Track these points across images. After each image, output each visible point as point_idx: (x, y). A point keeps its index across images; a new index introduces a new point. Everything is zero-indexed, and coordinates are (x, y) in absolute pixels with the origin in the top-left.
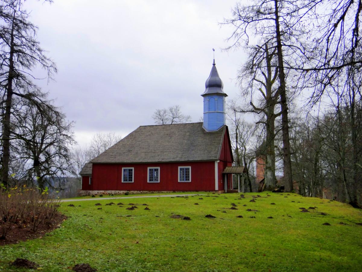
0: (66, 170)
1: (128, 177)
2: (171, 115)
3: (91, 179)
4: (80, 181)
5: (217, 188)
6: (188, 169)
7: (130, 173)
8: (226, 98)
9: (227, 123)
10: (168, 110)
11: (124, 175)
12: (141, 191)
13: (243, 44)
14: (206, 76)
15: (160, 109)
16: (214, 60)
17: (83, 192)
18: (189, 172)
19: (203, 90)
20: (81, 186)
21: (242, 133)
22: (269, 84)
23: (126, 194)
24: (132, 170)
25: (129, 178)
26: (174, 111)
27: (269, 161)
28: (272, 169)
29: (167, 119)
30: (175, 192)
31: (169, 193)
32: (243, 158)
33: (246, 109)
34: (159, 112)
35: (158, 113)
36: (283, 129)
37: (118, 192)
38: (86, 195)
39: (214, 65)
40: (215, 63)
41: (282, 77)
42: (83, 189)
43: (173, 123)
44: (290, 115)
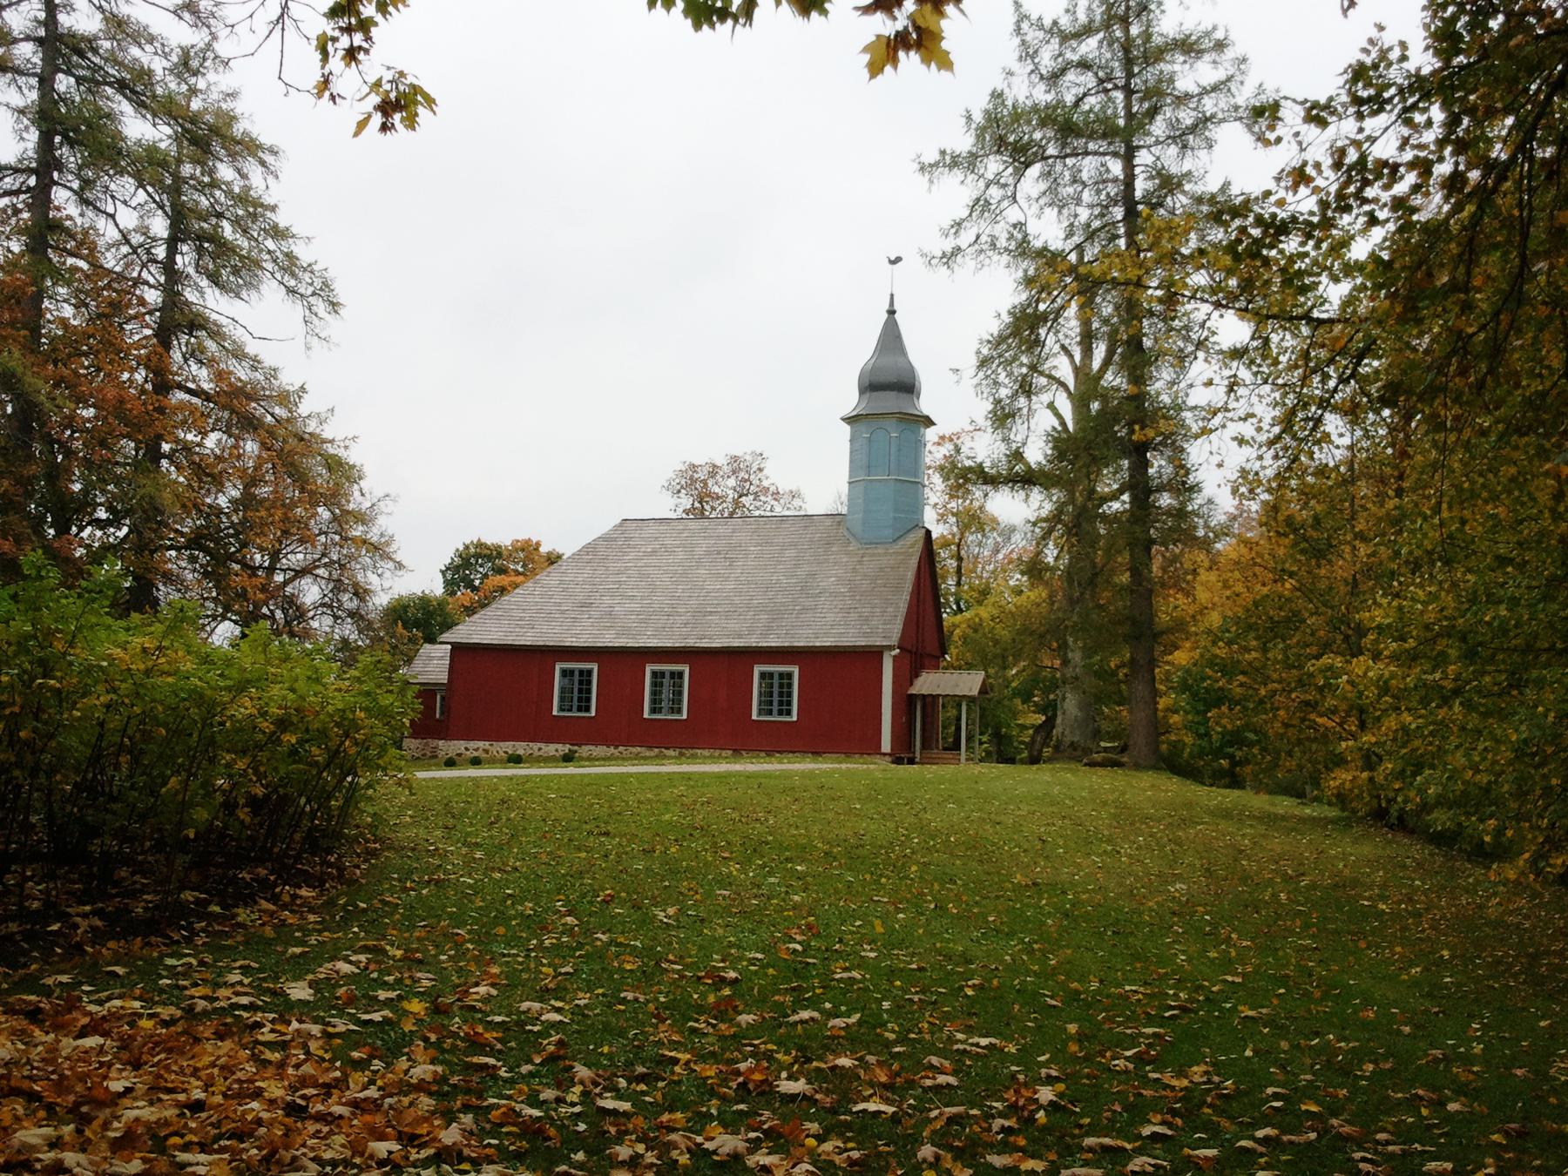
5: (886, 746)
6: (790, 675)
16: (892, 295)
18: (790, 685)
24: (590, 672)
37: (540, 749)
39: (892, 312)
40: (896, 307)
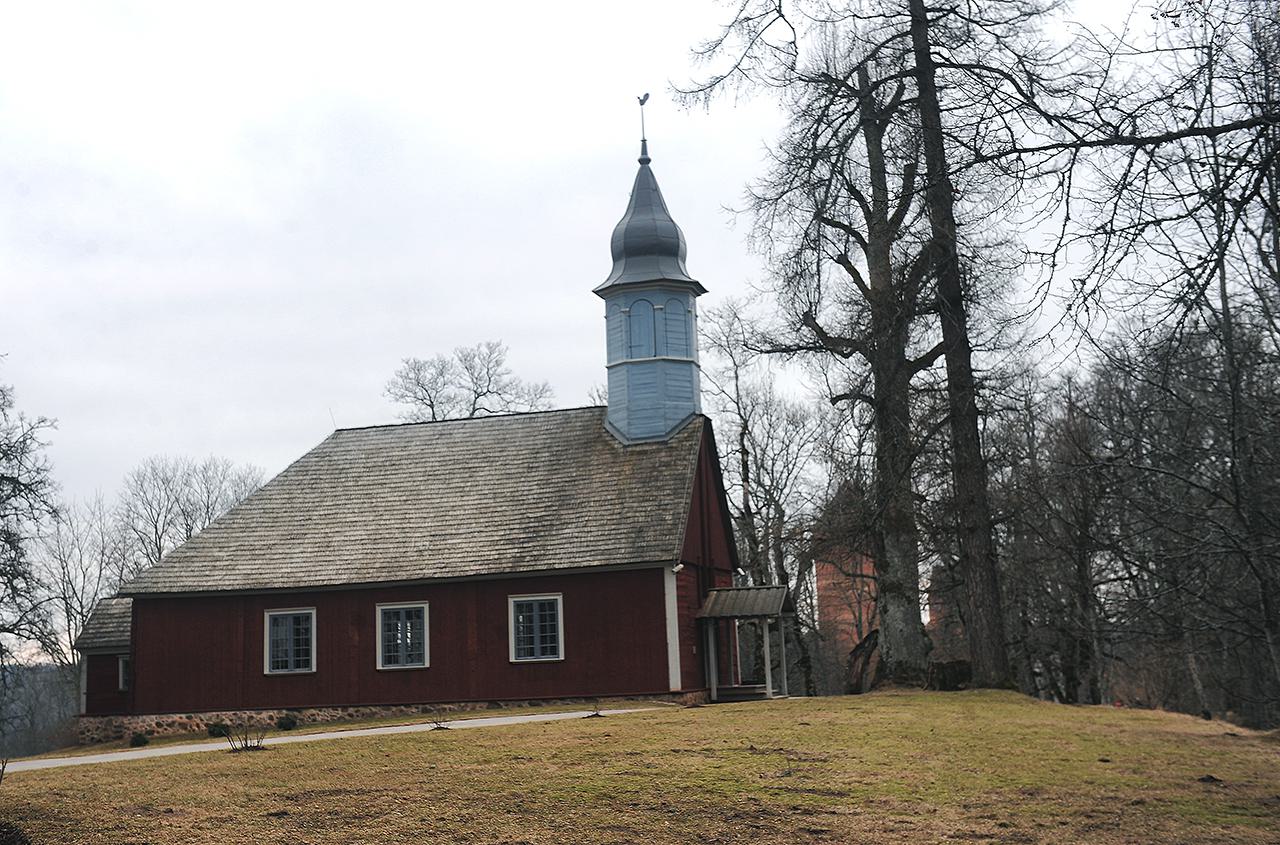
0: (12, 631)
1: (291, 647)
2: (466, 380)
3: (126, 663)
4: (78, 677)
5: (675, 682)
6: (552, 604)
7: (297, 632)
8: (698, 298)
9: (707, 408)
10: (456, 361)
11: (275, 644)
12: (351, 710)
13: (771, 66)
14: (613, 208)
15: (423, 357)
16: (644, 141)
17: (87, 722)
18: (554, 618)
19: (602, 268)
20: (84, 698)
21: (764, 451)
22: (884, 230)
23: (286, 726)
25: (297, 653)
26: (483, 367)
27: (895, 558)
28: (903, 591)
29: (449, 399)
30: (538, 705)
31: (463, 710)
32: (771, 552)
33: (789, 340)
34: (418, 367)
35: (412, 375)
36: (953, 419)
38: (107, 739)
39: (645, 161)
40: (650, 155)
41: (941, 197)
42: (93, 710)
43: (477, 414)
44: (982, 362)
